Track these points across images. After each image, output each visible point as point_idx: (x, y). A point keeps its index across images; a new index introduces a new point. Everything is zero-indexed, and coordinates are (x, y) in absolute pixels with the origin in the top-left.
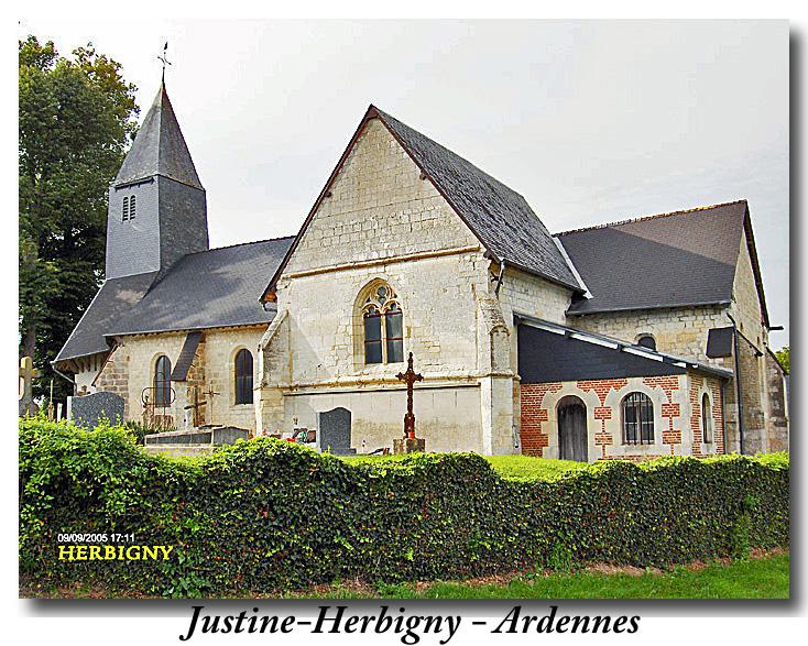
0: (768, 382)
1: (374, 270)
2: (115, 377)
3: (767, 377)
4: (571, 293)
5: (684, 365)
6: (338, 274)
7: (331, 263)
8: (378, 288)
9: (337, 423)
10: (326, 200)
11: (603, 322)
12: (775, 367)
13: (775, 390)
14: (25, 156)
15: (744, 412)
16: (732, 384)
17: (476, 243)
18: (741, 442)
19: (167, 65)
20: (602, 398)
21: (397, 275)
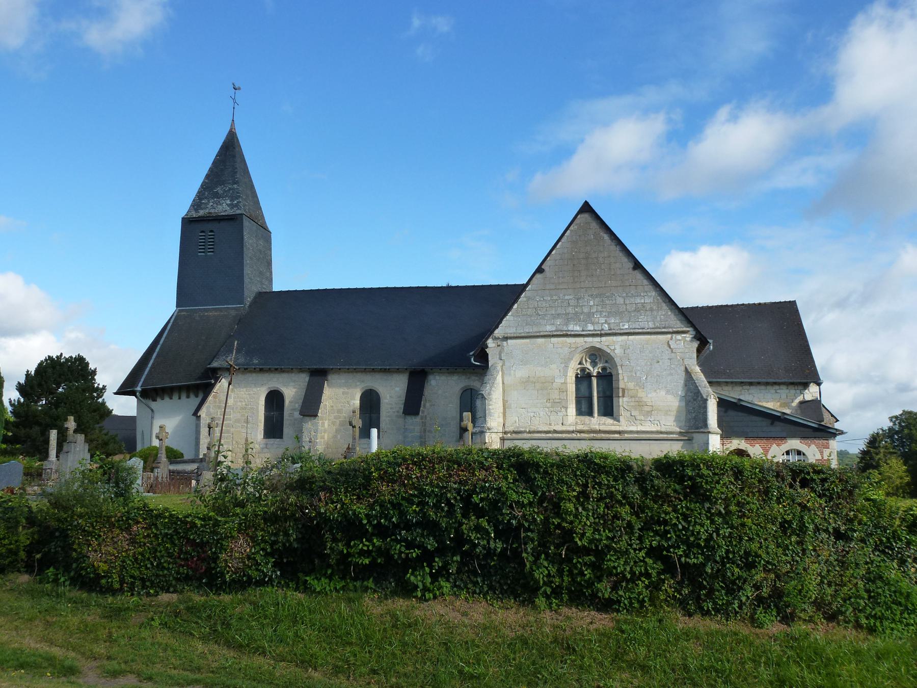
6: (553, 340)
10: (538, 276)
21: (614, 346)
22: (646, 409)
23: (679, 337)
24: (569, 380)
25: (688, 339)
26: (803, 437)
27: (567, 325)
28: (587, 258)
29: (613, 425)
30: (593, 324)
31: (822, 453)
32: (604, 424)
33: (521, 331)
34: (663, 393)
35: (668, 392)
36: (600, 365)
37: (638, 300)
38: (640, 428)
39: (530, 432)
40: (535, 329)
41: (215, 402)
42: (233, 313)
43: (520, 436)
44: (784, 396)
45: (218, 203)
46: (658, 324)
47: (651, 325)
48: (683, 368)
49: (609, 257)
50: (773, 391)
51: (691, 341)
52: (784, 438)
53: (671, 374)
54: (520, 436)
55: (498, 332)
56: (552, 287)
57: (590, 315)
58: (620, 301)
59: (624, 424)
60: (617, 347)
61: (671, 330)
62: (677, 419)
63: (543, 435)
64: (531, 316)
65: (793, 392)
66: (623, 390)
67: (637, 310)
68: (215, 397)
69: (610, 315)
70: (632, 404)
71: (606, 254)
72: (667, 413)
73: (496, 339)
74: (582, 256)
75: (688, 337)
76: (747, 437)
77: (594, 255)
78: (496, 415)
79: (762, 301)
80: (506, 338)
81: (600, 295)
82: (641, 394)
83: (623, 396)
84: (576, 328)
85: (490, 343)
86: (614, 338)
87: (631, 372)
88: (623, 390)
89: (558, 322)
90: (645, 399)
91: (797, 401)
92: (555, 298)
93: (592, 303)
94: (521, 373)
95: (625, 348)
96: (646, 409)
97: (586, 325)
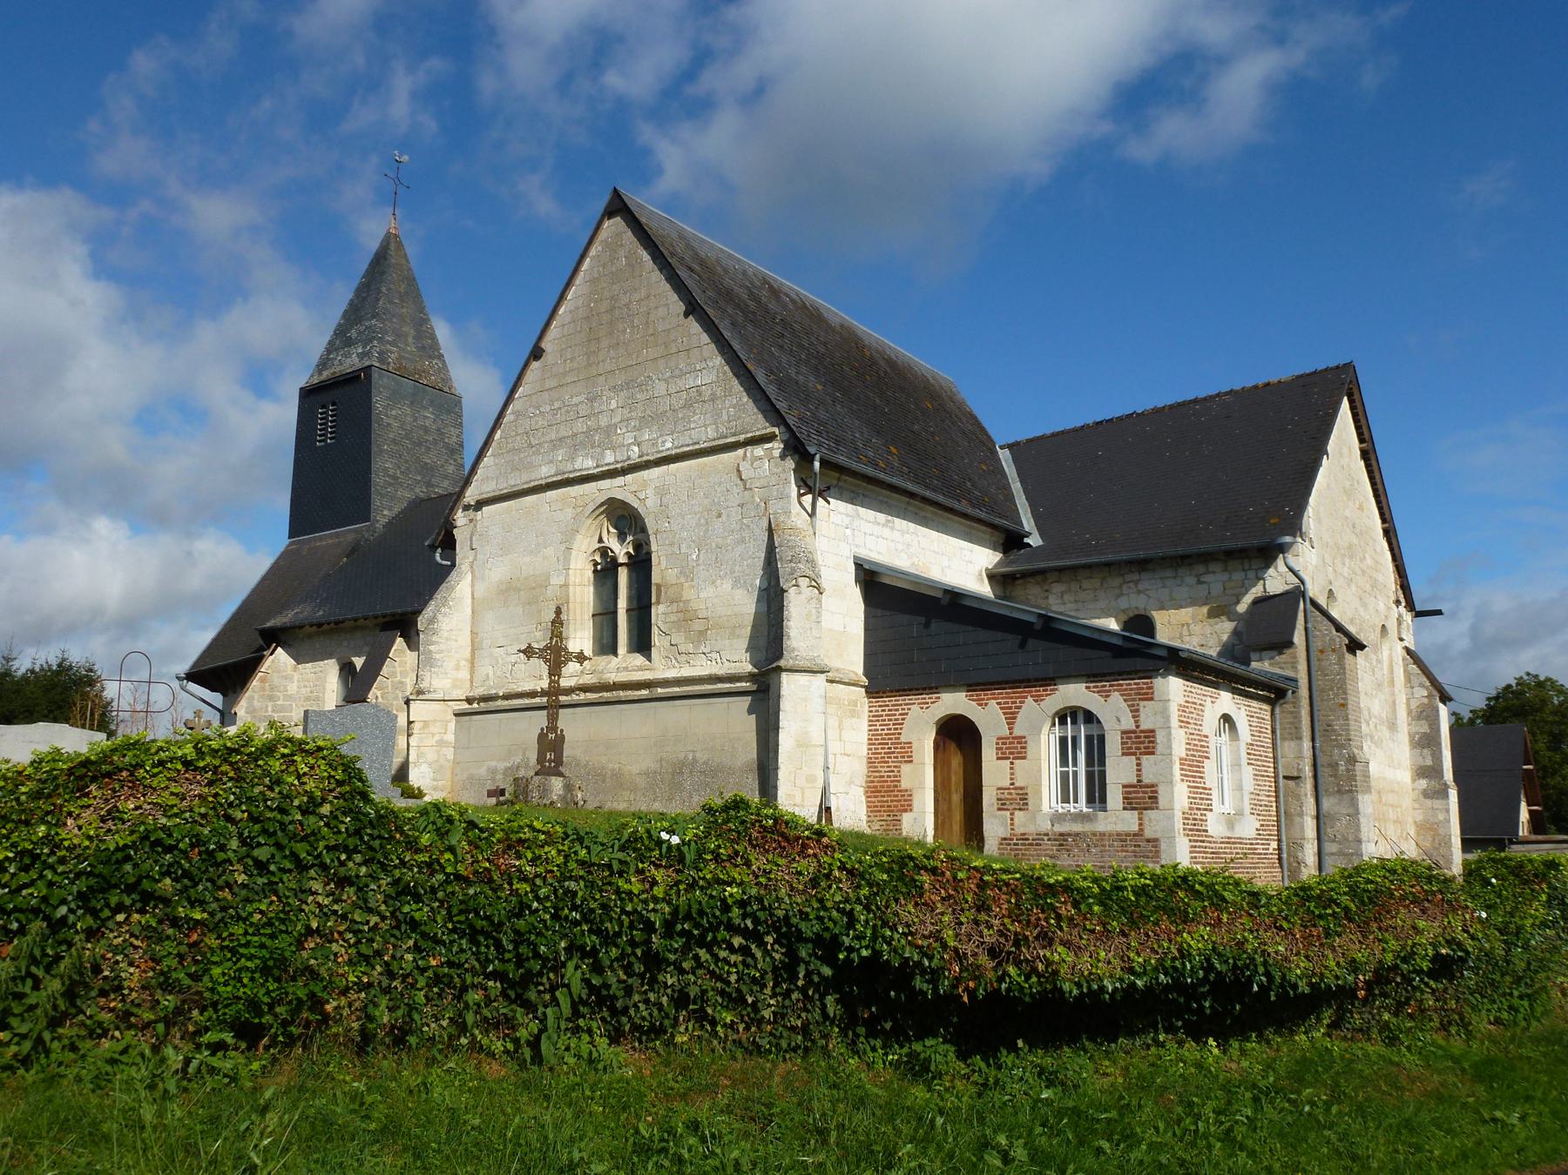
0: (1410, 712)
1: (605, 484)
2: (271, 698)
3: (1408, 705)
4: (1000, 537)
5: (1163, 653)
6: (551, 495)
7: (545, 472)
8: (624, 518)
9: (1241, 944)
10: (535, 365)
11: (1058, 588)
12: (1422, 685)
13: (1425, 729)
14: (1342, 747)
15: (1322, 760)
16: (1296, 704)
17: (762, 426)
18: (1318, 818)
19: (401, 190)
20: (1011, 718)
21: (639, 491)
22: (698, 626)
23: (759, 451)
24: (574, 578)
25: (777, 453)
26: (1092, 676)
27: (572, 459)
28: (613, 308)
29: (640, 669)
30: (613, 449)
31: (1135, 712)
32: (626, 669)
33: (504, 487)
34: (727, 585)
35: (736, 584)
36: (630, 538)
37: (691, 382)
38: (686, 672)
39: (506, 697)
40: (525, 478)
41: (263, 689)
42: (350, 537)
43: (492, 705)
44: (1217, 588)
45: (346, 356)
46: (723, 429)
47: (711, 433)
48: (766, 524)
49: (648, 297)
50: (1191, 580)
51: (783, 457)
52: (1047, 680)
53: (743, 541)
54: (492, 705)
55: (471, 495)
56: (553, 383)
57: (610, 430)
58: (660, 388)
59: (661, 667)
60: (650, 492)
61: (742, 438)
62: (751, 648)
63: (527, 701)
64: (519, 450)
65: (1238, 576)
66: (659, 586)
67: (688, 405)
68: (263, 680)
69: (645, 422)
70: (673, 618)
71: (643, 293)
72: (733, 633)
73: (467, 508)
74: (604, 306)
75: (777, 447)
76: (976, 685)
77: (624, 300)
78: (449, 665)
79: (1274, 379)
80: (480, 505)
81: (628, 385)
82: (688, 594)
83: (658, 603)
84: (586, 464)
85: (460, 518)
86: (645, 474)
87: (671, 544)
88: (659, 586)
89: (560, 455)
90: (694, 605)
91: (1248, 599)
92: (557, 405)
93: (614, 404)
94: (498, 572)
95: (661, 492)
96: (698, 626)
97: (602, 454)
